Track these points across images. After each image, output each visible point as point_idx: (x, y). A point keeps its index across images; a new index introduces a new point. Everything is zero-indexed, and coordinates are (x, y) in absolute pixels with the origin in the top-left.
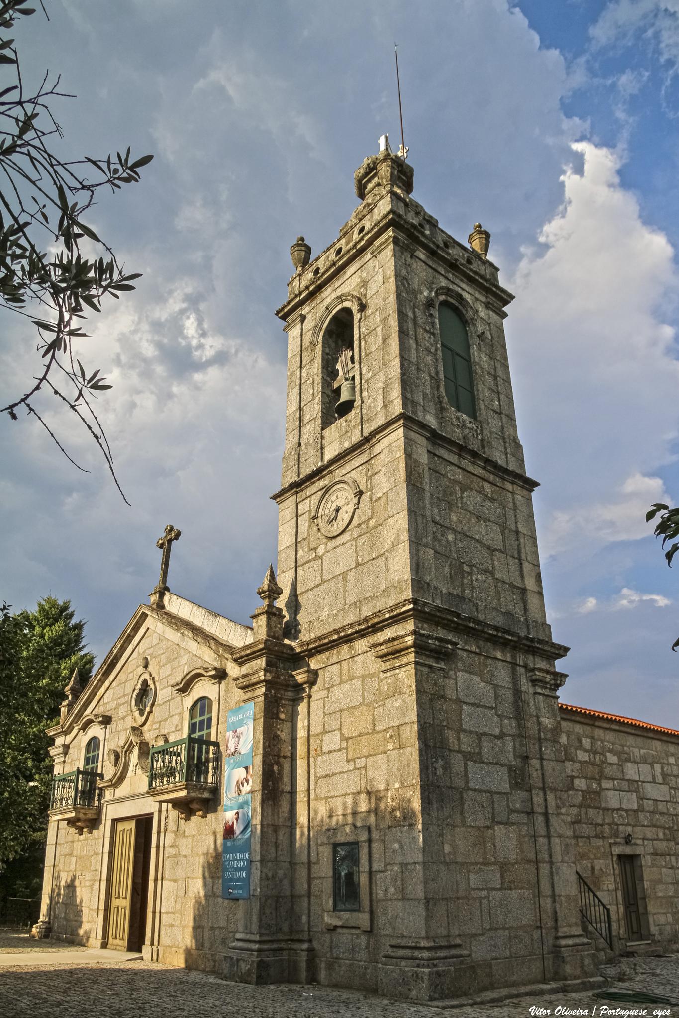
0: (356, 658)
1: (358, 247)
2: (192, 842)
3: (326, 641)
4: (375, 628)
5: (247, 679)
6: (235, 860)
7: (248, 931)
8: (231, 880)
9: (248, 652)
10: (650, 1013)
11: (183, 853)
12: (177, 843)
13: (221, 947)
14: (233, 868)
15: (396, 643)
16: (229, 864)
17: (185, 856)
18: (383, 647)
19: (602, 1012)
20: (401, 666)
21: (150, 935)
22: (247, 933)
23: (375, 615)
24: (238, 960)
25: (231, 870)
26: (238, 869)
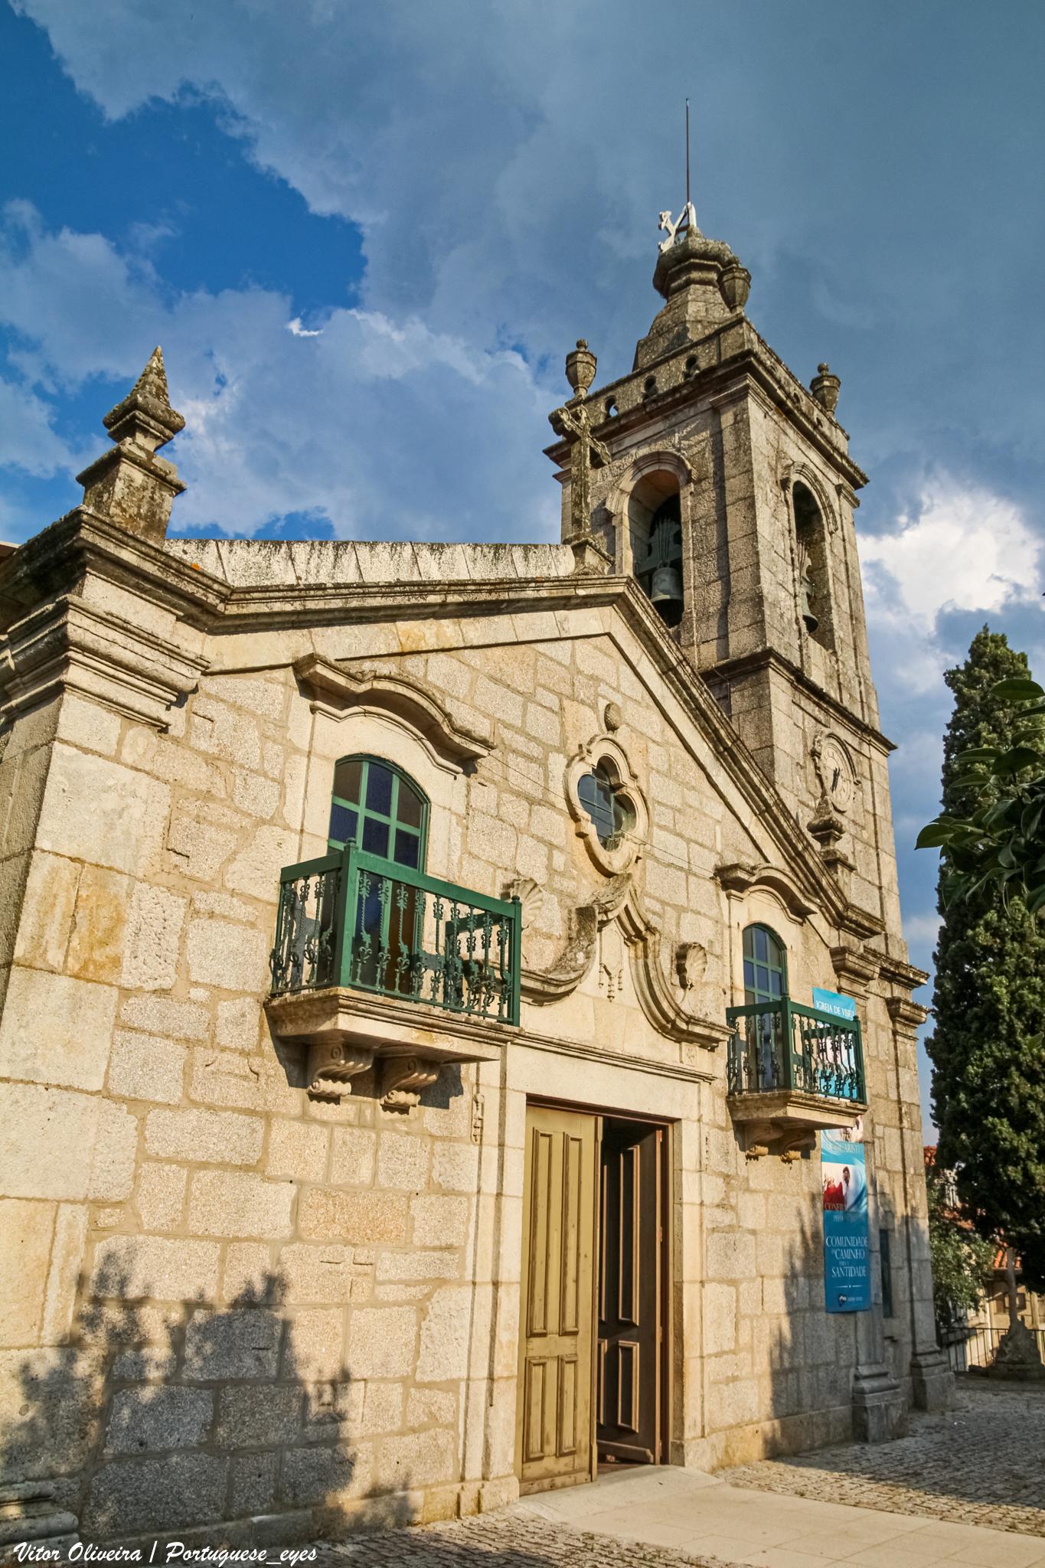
2: (766, 1205)
5: (862, 963)
6: (850, 1247)
7: (872, 1360)
8: (844, 1280)
9: (866, 924)
11: (749, 1224)
12: (733, 1201)
13: (829, 1397)
14: (846, 1260)
16: (839, 1253)
17: (754, 1232)
19: (170, 1555)
22: (871, 1364)
24: (887, 1408)
25: (843, 1263)
26: (852, 1262)
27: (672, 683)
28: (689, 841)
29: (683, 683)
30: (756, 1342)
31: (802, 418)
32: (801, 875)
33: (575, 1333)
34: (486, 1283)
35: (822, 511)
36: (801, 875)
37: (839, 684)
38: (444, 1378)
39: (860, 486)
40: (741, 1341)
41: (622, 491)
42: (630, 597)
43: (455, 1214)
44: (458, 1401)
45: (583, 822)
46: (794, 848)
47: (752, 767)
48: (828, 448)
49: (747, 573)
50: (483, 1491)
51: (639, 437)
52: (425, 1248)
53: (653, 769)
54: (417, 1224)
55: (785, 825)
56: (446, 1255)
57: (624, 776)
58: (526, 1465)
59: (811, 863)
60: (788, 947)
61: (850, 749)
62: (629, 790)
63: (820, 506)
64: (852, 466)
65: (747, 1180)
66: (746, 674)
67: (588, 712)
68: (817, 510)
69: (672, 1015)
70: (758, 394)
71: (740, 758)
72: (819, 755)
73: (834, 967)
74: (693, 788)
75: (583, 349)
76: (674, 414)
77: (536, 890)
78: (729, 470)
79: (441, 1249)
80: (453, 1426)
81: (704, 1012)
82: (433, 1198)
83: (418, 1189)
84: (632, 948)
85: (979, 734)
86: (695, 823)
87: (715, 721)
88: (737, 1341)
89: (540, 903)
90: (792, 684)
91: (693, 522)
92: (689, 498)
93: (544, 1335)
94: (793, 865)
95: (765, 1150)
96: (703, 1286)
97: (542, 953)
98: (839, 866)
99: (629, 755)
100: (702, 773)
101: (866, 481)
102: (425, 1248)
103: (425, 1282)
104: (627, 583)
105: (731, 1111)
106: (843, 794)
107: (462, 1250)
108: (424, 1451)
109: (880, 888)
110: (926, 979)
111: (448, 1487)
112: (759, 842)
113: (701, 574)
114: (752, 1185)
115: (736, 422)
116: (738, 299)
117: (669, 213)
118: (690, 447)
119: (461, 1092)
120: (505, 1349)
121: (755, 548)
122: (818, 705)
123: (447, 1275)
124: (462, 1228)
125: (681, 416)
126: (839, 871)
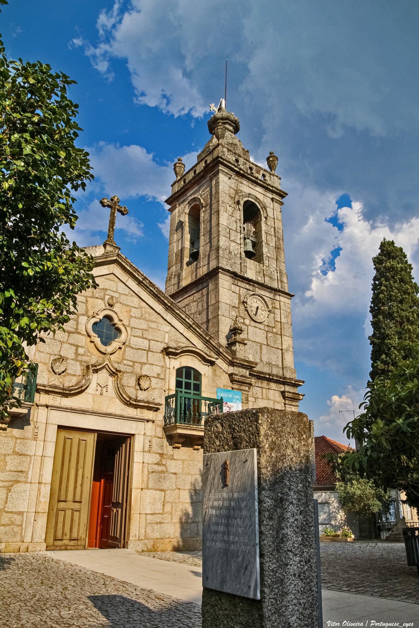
0: (270, 390)
1: (269, 187)
3: (262, 375)
4: (284, 383)
9: (246, 364)
10: (401, 624)
15: (296, 396)
17: (175, 474)
18: (291, 394)
19: (372, 624)
20: (294, 406)
21: (65, 489)
23: (290, 379)
27: (143, 286)
28: (149, 340)
29: (146, 286)
30: (173, 511)
31: (249, 176)
32: (211, 348)
33: (81, 502)
34: (36, 483)
35: (261, 210)
36: (211, 348)
37: (264, 274)
38: (17, 511)
39: (285, 197)
40: (165, 510)
41: (186, 213)
42: (120, 260)
43: (24, 462)
44: (23, 518)
45: (92, 338)
46: (205, 339)
47: (181, 312)
48: (265, 185)
49: (216, 239)
50: (29, 546)
51: (191, 192)
52: (11, 471)
53: (133, 317)
54: (8, 464)
55: (199, 331)
56: (20, 474)
57: (116, 321)
58: (55, 541)
59: (214, 344)
60: (203, 374)
61: (264, 297)
62: (118, 325)
63: (260, 208)
64: (278, 190)
65: (173, 455)
66: (213, 276)
67: (100, 301)
68: (259, 210)
69: (128, 399)
70: (224, 171)
71: (175, 309)
72: (246, 303)
73: (230, 380)
74: (154, 322)
75: (180, 162)
76: (200, 182)
77: (64, 361)
78: (213, 202)
79: (18, 471)
80: (21, 525)
81: (153, 398)
82: (15, 456)
83: (9, 453)
84: (113, 378)
85: (382, 282)
86: (153, 333)
87: (162, 298)
88: (163, 510)
89: (66, 365)
90: (232, 278)
91: (204, 222)
92: (203, 213)
93: (66, 501)
94: (207, 345)
95: (181, 445)
96: (142, 490)
97: (70, 381)
98: (237, 344)
99: (118, 314)
100: (159, 316)
101: (287, 194)
102: (11, 471)
103: (10, 481)
104: (117, 256)
105: (165, 432)
106: (261, 316)
107: (27, 473)
108: (8, 532)
109: (282, 350)
110: (303, 383)
111: (16, 543)
112: (188, 338)
113: (205, 241)
114: (175, 457)
115: (216, 183)
116: (220, 136)
117: (213, 104)
118: (204, 194)
119: (30, 424)
120: (43, 504)
121: (218, 229)
122: (248, 284)
123: (20, 479)
124: (28, 466)
125: (202, 183)
126: (237, 346)
